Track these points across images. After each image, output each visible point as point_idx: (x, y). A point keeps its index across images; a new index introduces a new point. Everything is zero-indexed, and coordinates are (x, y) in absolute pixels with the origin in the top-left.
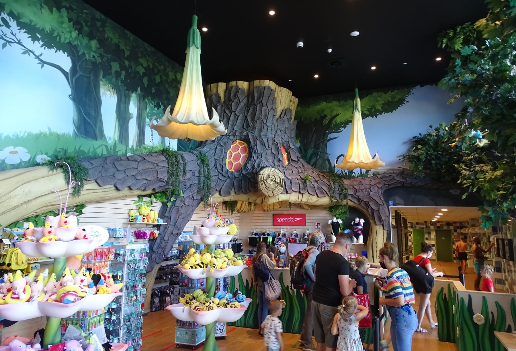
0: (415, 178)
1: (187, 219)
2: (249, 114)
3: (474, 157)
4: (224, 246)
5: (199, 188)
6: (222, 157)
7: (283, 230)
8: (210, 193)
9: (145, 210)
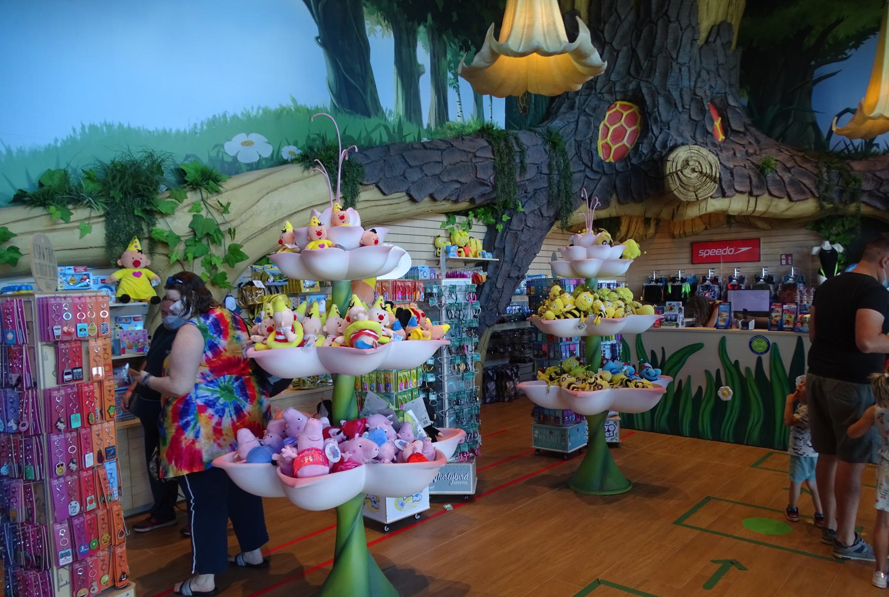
1: (532, 253)
2: (641, 43)
5: (550, 196)
6: (590, 135)
8: (571, 204)
9: (461, 237)
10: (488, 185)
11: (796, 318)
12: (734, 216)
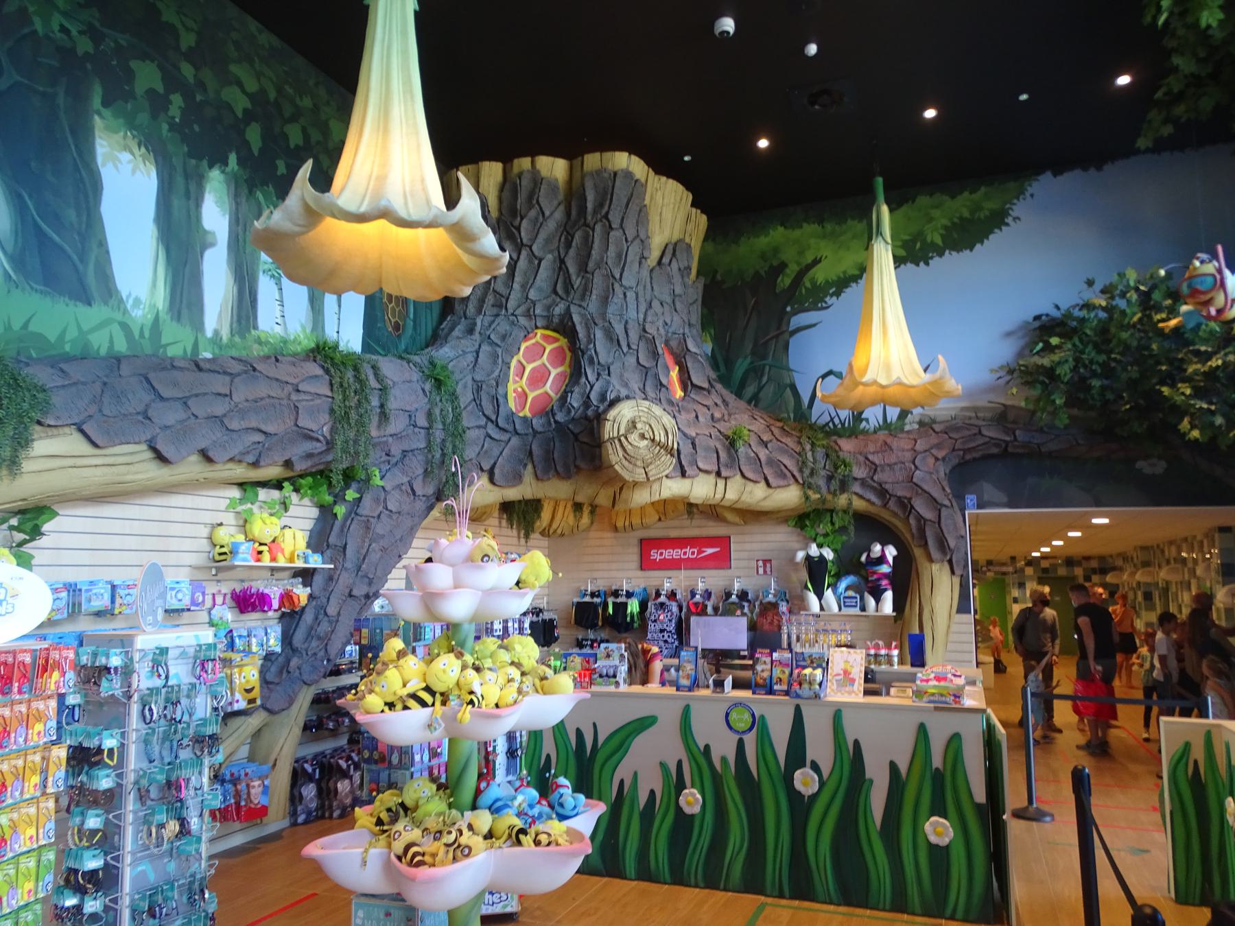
0: (1041, 430)
2: (572, 252)
3: (1224, 363)
4: (506, 629)
5: (429, 462)
6: (496, 373)
7: (669, 581)
9: (265, 526)
10: (318, 440)
11: (791, 674)
12: (697, 505)
